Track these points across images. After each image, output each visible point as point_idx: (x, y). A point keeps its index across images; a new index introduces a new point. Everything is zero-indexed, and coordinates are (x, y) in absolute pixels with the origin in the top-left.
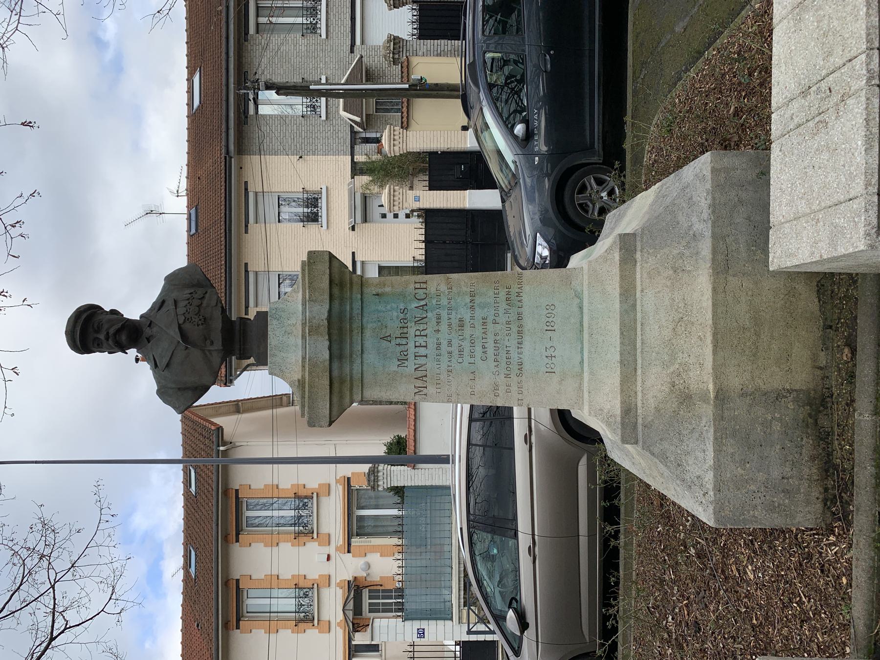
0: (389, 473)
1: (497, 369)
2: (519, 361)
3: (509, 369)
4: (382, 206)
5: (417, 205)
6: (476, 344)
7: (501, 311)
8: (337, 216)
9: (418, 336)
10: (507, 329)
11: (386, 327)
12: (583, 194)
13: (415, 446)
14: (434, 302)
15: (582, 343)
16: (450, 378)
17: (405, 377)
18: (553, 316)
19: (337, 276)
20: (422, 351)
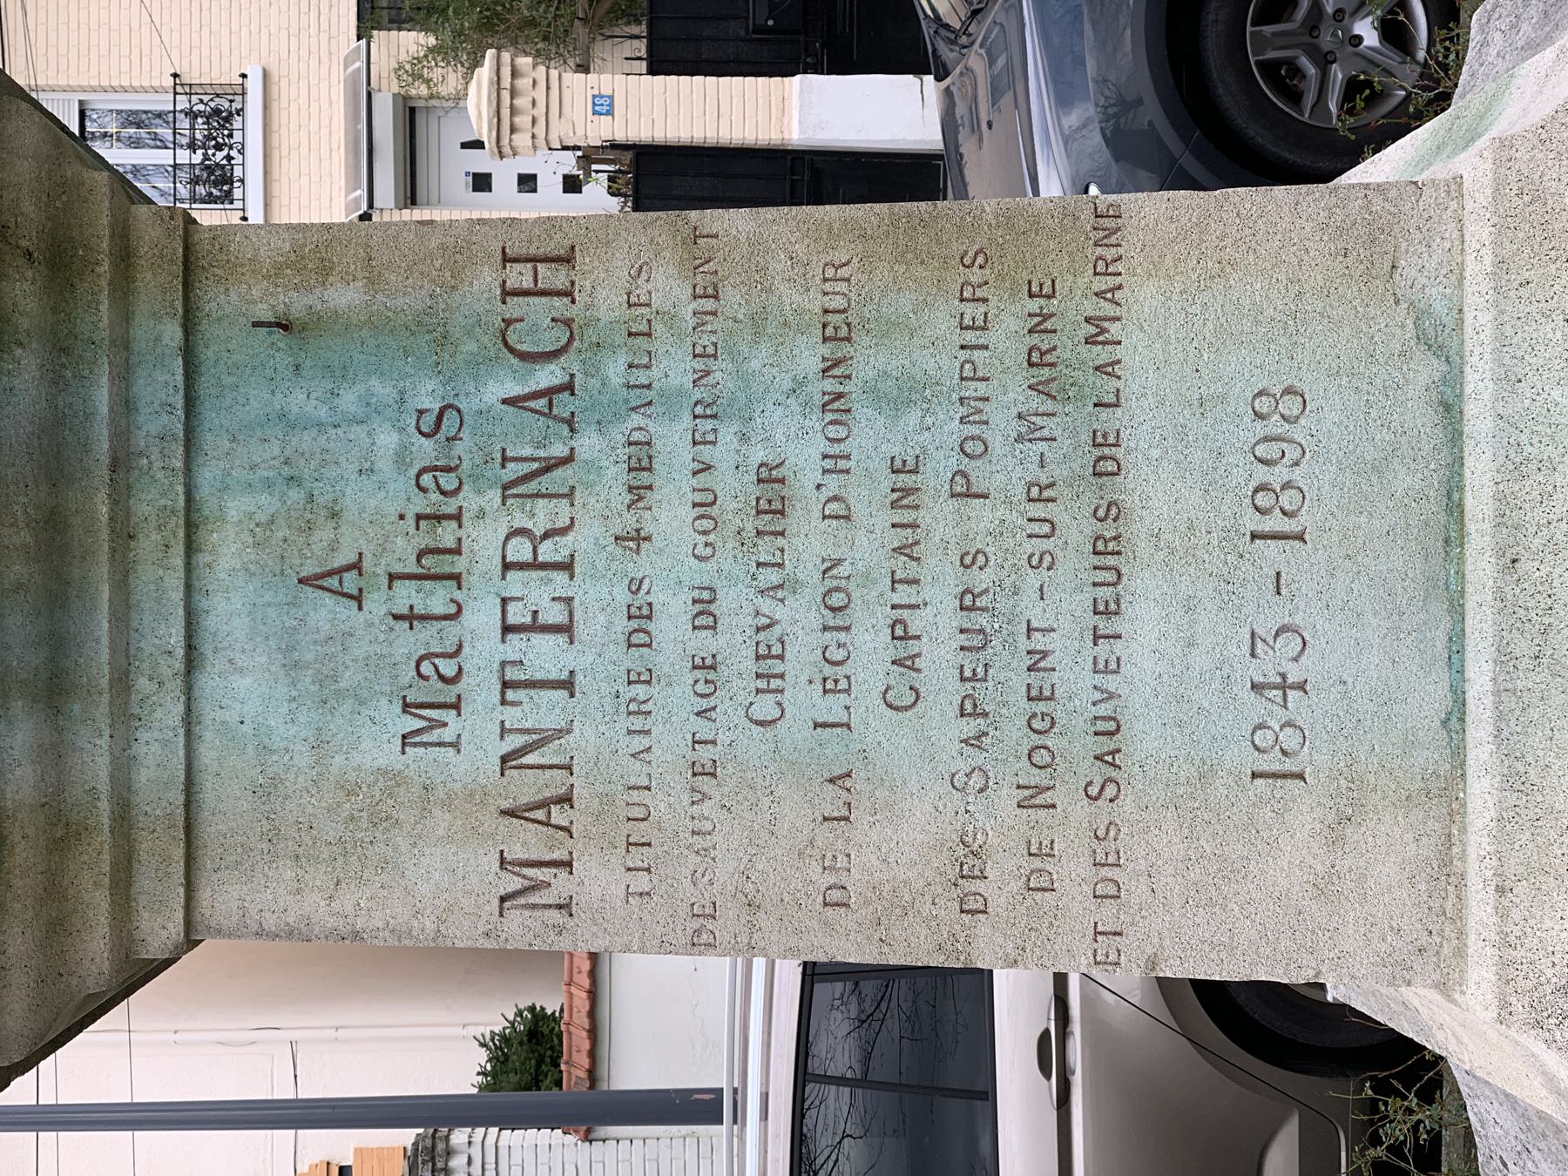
0: (490, 1158)
1: (979, 758)
2: (1103, 710)
3: (1042, 757)
4: (478, 145)
5: (599, 131)
6: (857, 613)
7: (1001, 424)
8: (304, 180)
9: (521, 566)
10: (1036, 528)
11: (334, 515)
12: (1277, 21)
13: (593, 1054)
14: (615, 369)
15: (1457, 610)
16: (706, 808)
17: (448, 803)
18: (1292, 453)
19: (28, 207)
20: (545, 655)
